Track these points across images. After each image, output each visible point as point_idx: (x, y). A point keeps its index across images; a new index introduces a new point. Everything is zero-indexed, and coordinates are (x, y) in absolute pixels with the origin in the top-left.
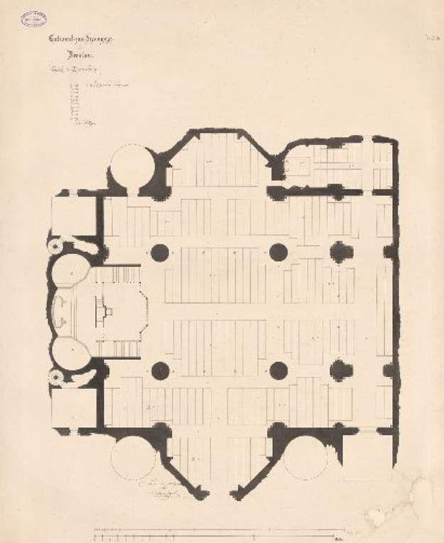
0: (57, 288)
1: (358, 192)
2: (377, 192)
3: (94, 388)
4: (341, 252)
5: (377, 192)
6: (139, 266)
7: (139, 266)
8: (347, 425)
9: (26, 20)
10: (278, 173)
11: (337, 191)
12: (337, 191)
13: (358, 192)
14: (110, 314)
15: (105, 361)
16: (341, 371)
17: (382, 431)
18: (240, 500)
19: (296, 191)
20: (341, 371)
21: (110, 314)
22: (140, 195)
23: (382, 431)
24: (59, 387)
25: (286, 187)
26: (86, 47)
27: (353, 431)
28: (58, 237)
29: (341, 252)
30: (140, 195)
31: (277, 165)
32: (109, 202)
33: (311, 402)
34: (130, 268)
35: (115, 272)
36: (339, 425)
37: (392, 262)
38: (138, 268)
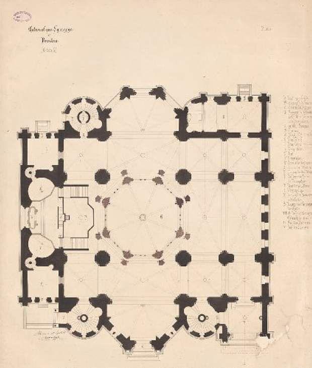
0: (31, 201)
1: (237, 135)
2: (251, 135)
3: (27, 272)
4: (226, 177)
5: (251, 135)
6: (87, 186)
7: (87, 186)
8: (230, 295)
9: (17, 17)
10: (183, 123)
11: (223, 135)
12: (223, 135)
13: (237, 135)
14: (57, 218)
15: (65, 252)
16: (226, 258)
17: (255, 300)
18: (208, 300)
19: (196, 135)
20: (226, 258)
21: (57, 218)
22: (88, 137)
23: (255, 300)
24: (32, 269)
25: (259, 253)
26: (54, 35)
27: (234, 299)
28: (32, 166)
29: (226, 177)
30: (88, 137)
31: (182, 114)
32: (67, 142)
33: (204, 280)
34: (80, 187)
35: (87, 194)
36: (225, 295)
37: (259, 296)
38: (87, 187)
